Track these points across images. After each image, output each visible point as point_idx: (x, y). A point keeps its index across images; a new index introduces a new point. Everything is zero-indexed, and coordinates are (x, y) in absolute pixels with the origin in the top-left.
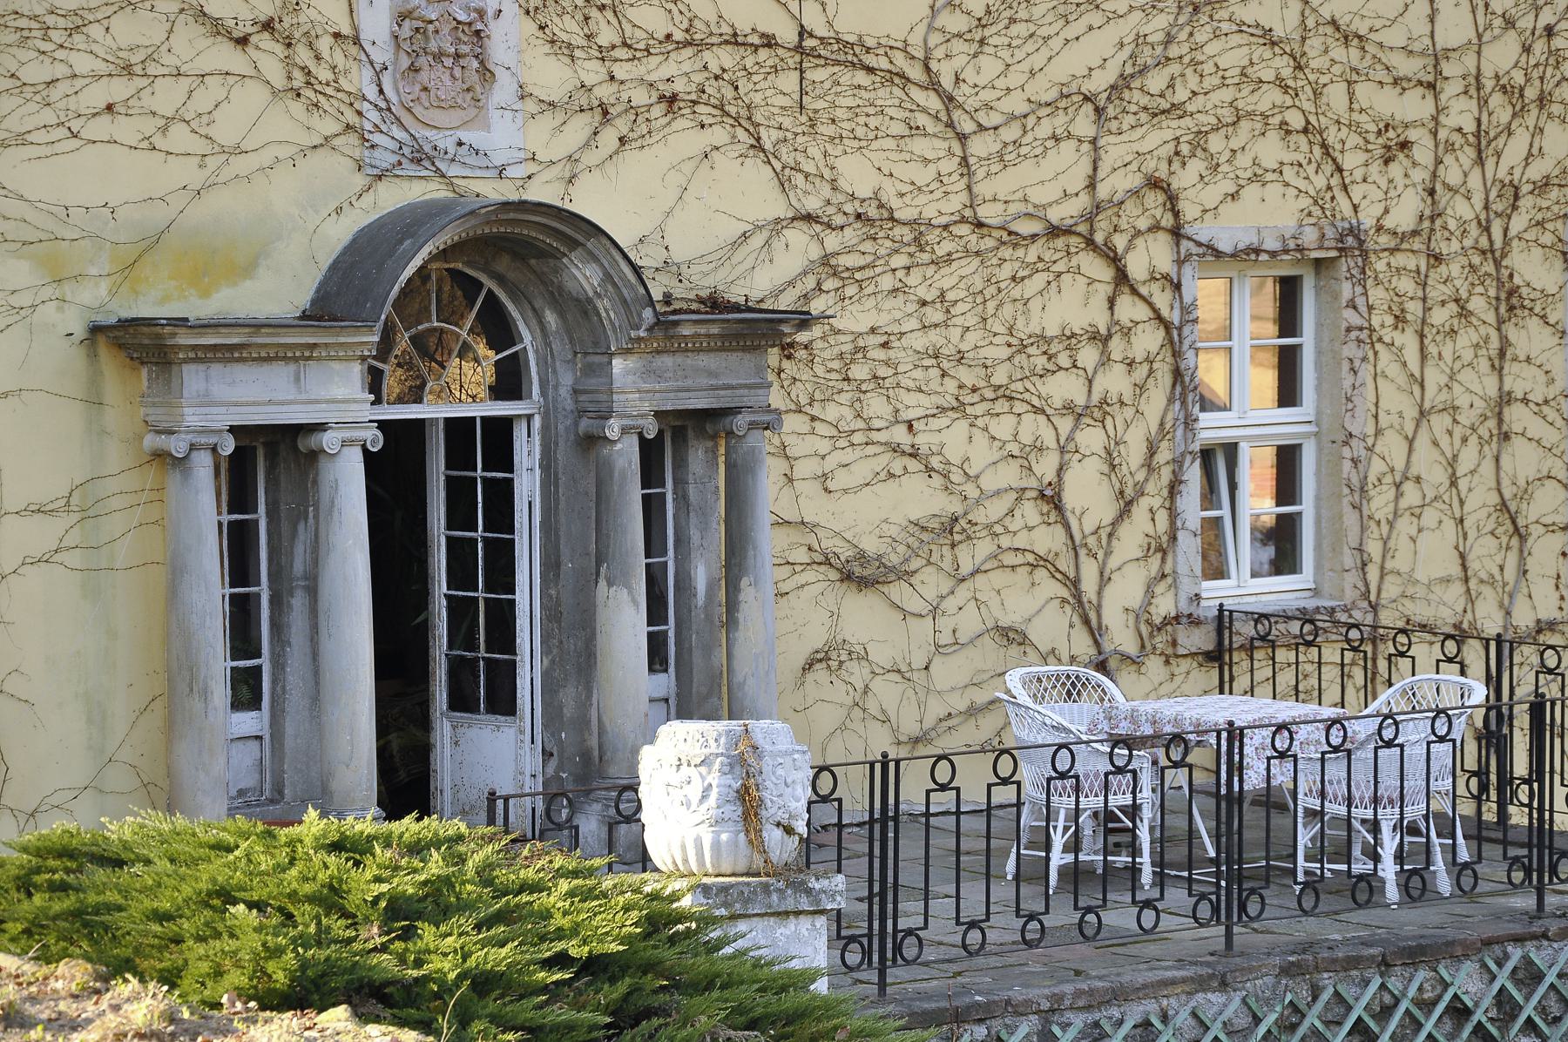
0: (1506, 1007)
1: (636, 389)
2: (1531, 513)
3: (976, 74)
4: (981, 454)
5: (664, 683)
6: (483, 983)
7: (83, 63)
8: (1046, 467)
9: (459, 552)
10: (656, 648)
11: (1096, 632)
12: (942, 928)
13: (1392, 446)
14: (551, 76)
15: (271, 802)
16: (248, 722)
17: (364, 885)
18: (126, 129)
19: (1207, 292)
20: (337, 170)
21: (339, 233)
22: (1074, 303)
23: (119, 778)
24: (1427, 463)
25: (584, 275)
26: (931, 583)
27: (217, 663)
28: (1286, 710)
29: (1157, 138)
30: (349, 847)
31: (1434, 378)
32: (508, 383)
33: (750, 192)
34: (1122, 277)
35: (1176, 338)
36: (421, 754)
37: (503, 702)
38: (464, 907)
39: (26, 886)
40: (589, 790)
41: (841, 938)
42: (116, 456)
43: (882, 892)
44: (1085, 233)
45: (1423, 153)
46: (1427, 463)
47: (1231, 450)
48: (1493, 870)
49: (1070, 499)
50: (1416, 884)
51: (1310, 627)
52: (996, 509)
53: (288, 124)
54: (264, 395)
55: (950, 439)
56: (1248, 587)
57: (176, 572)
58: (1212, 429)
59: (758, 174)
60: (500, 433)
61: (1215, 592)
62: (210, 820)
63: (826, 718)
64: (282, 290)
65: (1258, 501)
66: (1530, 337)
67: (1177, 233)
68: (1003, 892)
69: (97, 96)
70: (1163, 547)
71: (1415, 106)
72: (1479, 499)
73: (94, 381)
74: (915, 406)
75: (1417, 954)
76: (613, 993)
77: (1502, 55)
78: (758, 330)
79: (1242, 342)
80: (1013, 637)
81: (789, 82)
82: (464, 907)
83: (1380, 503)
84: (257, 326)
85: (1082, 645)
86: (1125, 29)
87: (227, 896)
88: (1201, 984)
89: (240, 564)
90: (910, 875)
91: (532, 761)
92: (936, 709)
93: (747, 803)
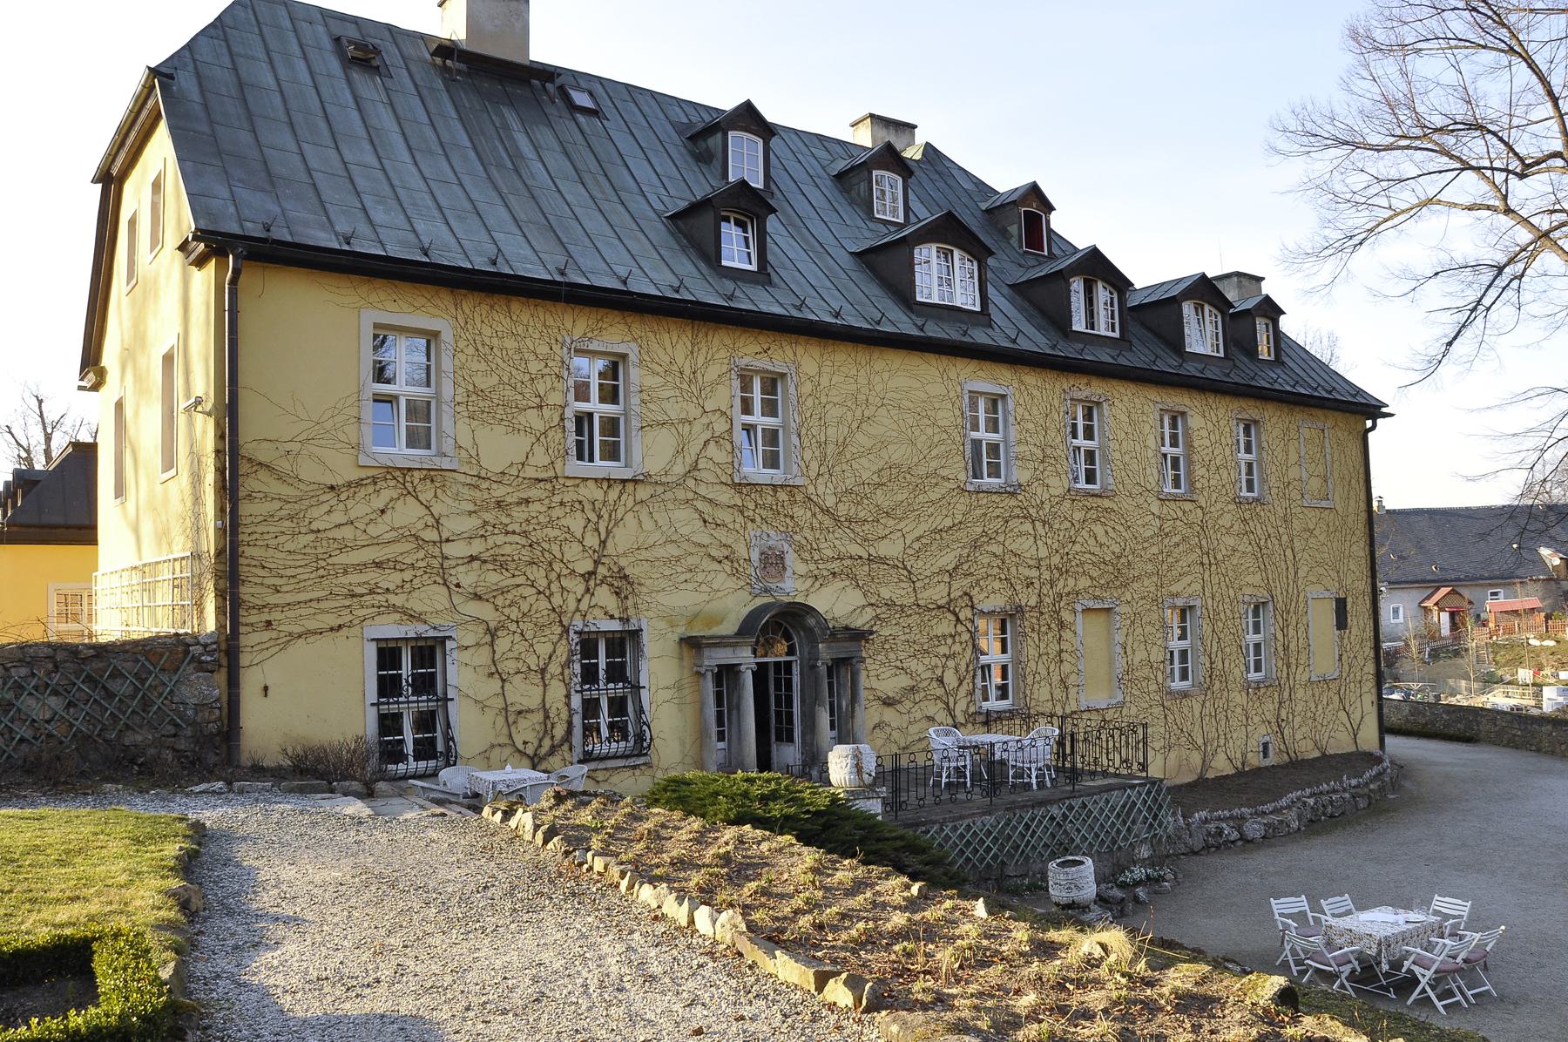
0: (1065, 816)
1: (825, 652)
2: (1069, 682)
3: (918, 566)
4: (921, 669)
5: (834, 733)
6: (787, 818)
7: (679, 569)
8: (939, 672)
9: (778, 698)
10: (832, 722)
11: (953, 717)
12: (913, 800)
13: (1032, 664)
14: (802, 568)
15: (728, 767)
16: (721, 745)
17: (755, 791)
18: (690, 586)
19: (981, 623)
20: (744, 595)
21: (745, 611)
22: (945, 626)
23: (688, 760)
24: (1041, 668)
25: (811, 622)
26: (908, 704)
27: (714, 729)
28: (1006, 738)
29: (966, 582)
30: (751, 781)
31: (1042, 645)
32: (791, 652)
33: (855, 598)
34: (958, 620)
35: (1100, 782)
36: (769, 753)
37: (790, 739)
38: (781, 797)
39: (665, 790)
40: (815, 764)
41: (885, 804)
42: (686, 673)
43: (896, 791)
44: (948, 608)
45: (1037, 585)
46: (1041, 668)
47: (989, 666)
48: (1062, 780)
49: (946, 680)
50: (1041, 785)
51: (1011, 714)
52: (925, 684)
53: (732, 583)
54: (725, 656)
55: (913, 664)
56: (994, 704)
57: (702, 704)
58: (984, 660)
59: (858, 593)
60: (788, 664)
61: (986, 705)
62: (711, 773)
63: (879, 742)
64: (729, 627)
65: (997, 680)
66: (1067, 634)
67: (972, 607)
68: (929, 790)
69: (683, 577)
70: (971, 693)
71: (1034, 573)
72: (1056, 679)
73: (681, 653)
74: (902, 655)
75: (1042, 803)
76: (822, 821)
77: (1056, 560)
78: (859, 636)
79: (991, 636)
80: (931, 719)
81: (866, 568)
82: (781, 797)
83: (1029, 680)
84: (723, 637)
85: (950, 721)
86: (957, 553)
87: (717, 794)
88: (984, 814)
89: (719, 703)
90: (904, 785)
91: (798, 756)
92: (910, 739)
93: (858, 768)
